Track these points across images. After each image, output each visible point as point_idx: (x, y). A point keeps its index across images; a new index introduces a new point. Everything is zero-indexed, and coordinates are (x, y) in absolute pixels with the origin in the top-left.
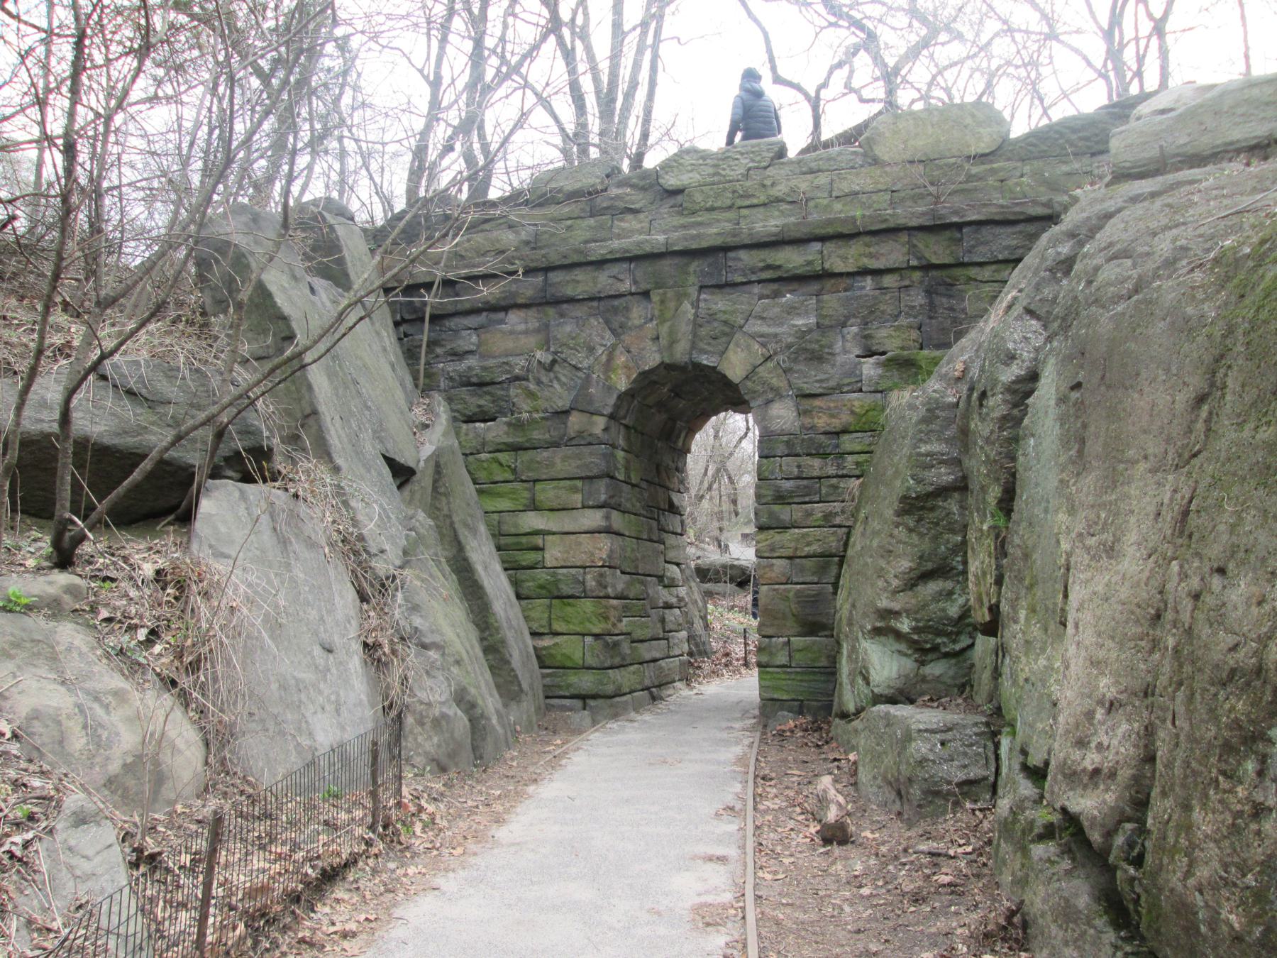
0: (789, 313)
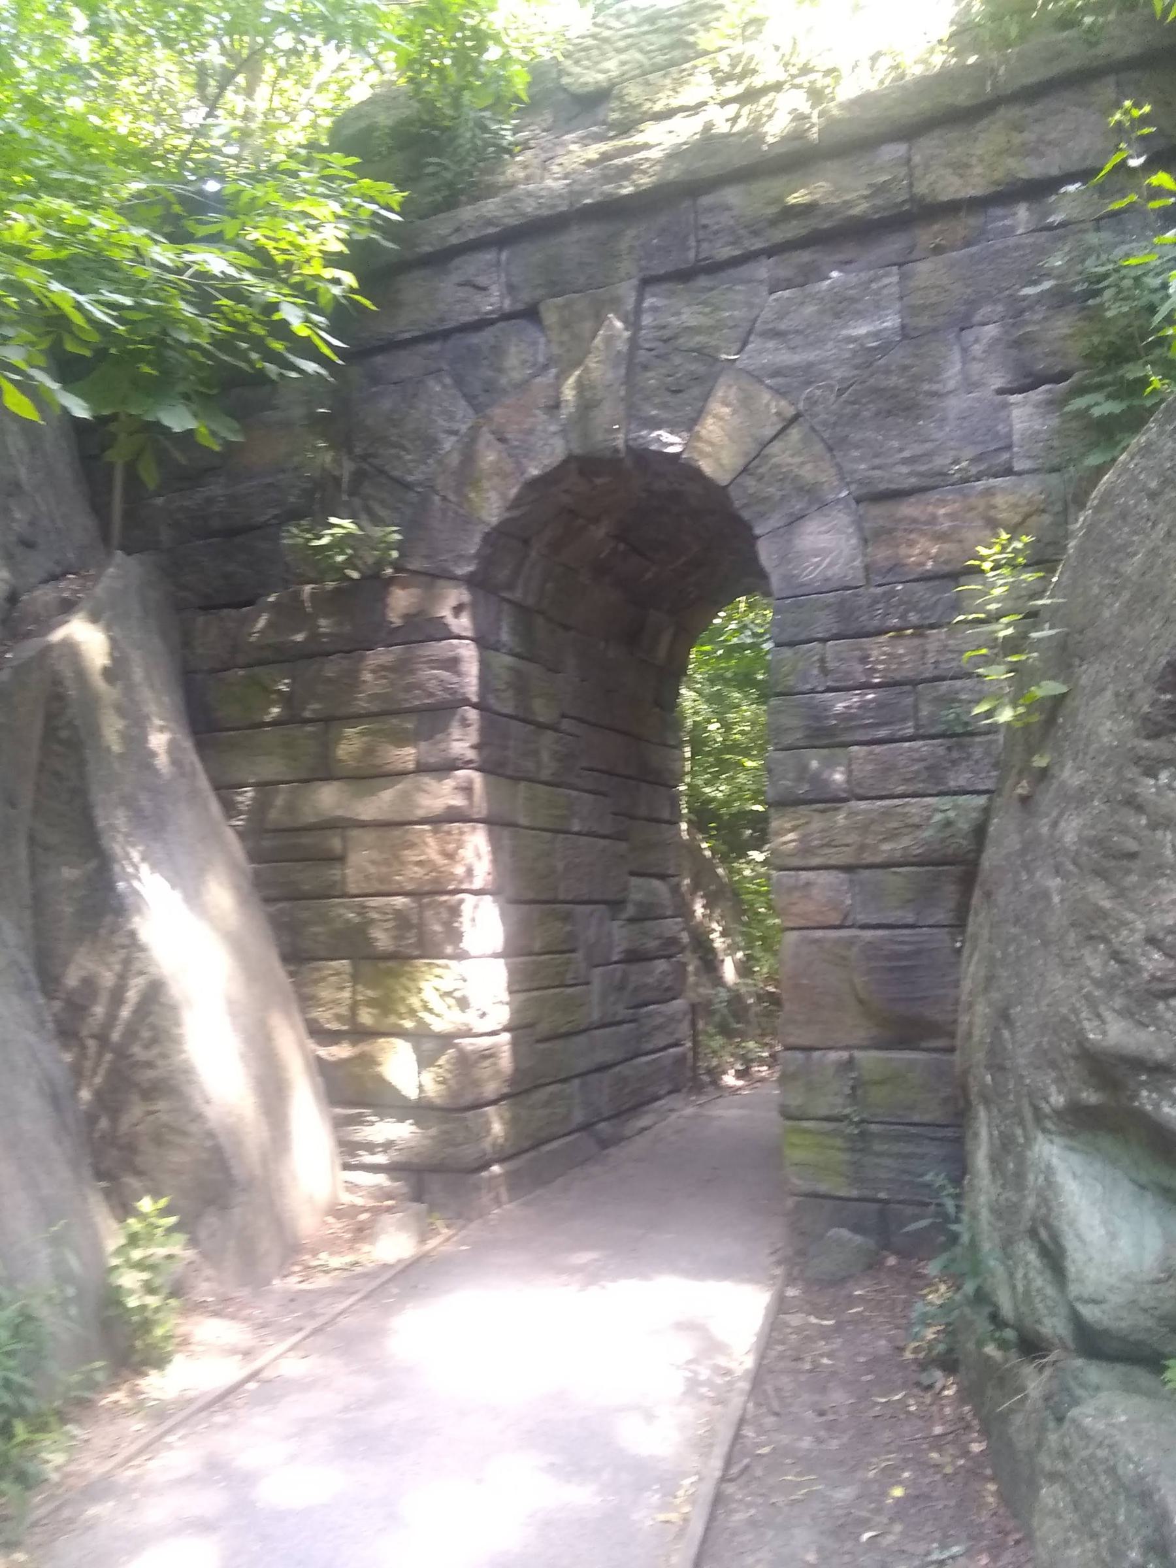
0: (837, 315)
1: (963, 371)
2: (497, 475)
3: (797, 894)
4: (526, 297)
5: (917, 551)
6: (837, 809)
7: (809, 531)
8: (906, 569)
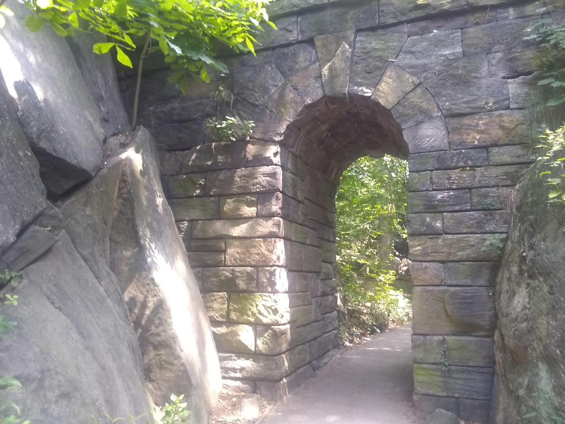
0: (436, 46)
2: (294, 102)
3: (421, 271)
4: (308, 35)
5: (471, 137)
6: (438, 238)
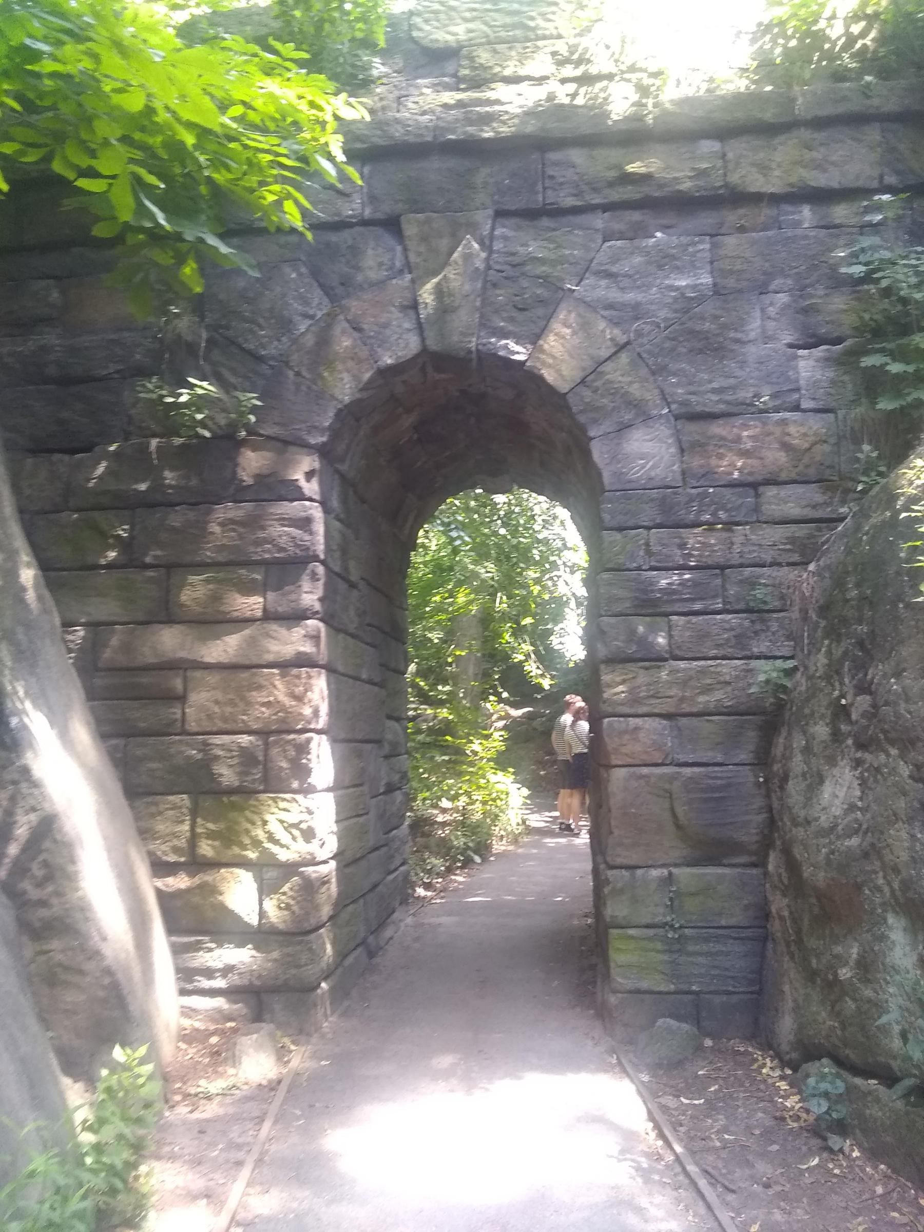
0: (660, 267)
1: (763, 327)
2: (352, 359)
3: (627, 737)
4: (386, 209)
5: (725, 463)
6: (659, 667)
7: (635, 438)
8: (716, 476)
